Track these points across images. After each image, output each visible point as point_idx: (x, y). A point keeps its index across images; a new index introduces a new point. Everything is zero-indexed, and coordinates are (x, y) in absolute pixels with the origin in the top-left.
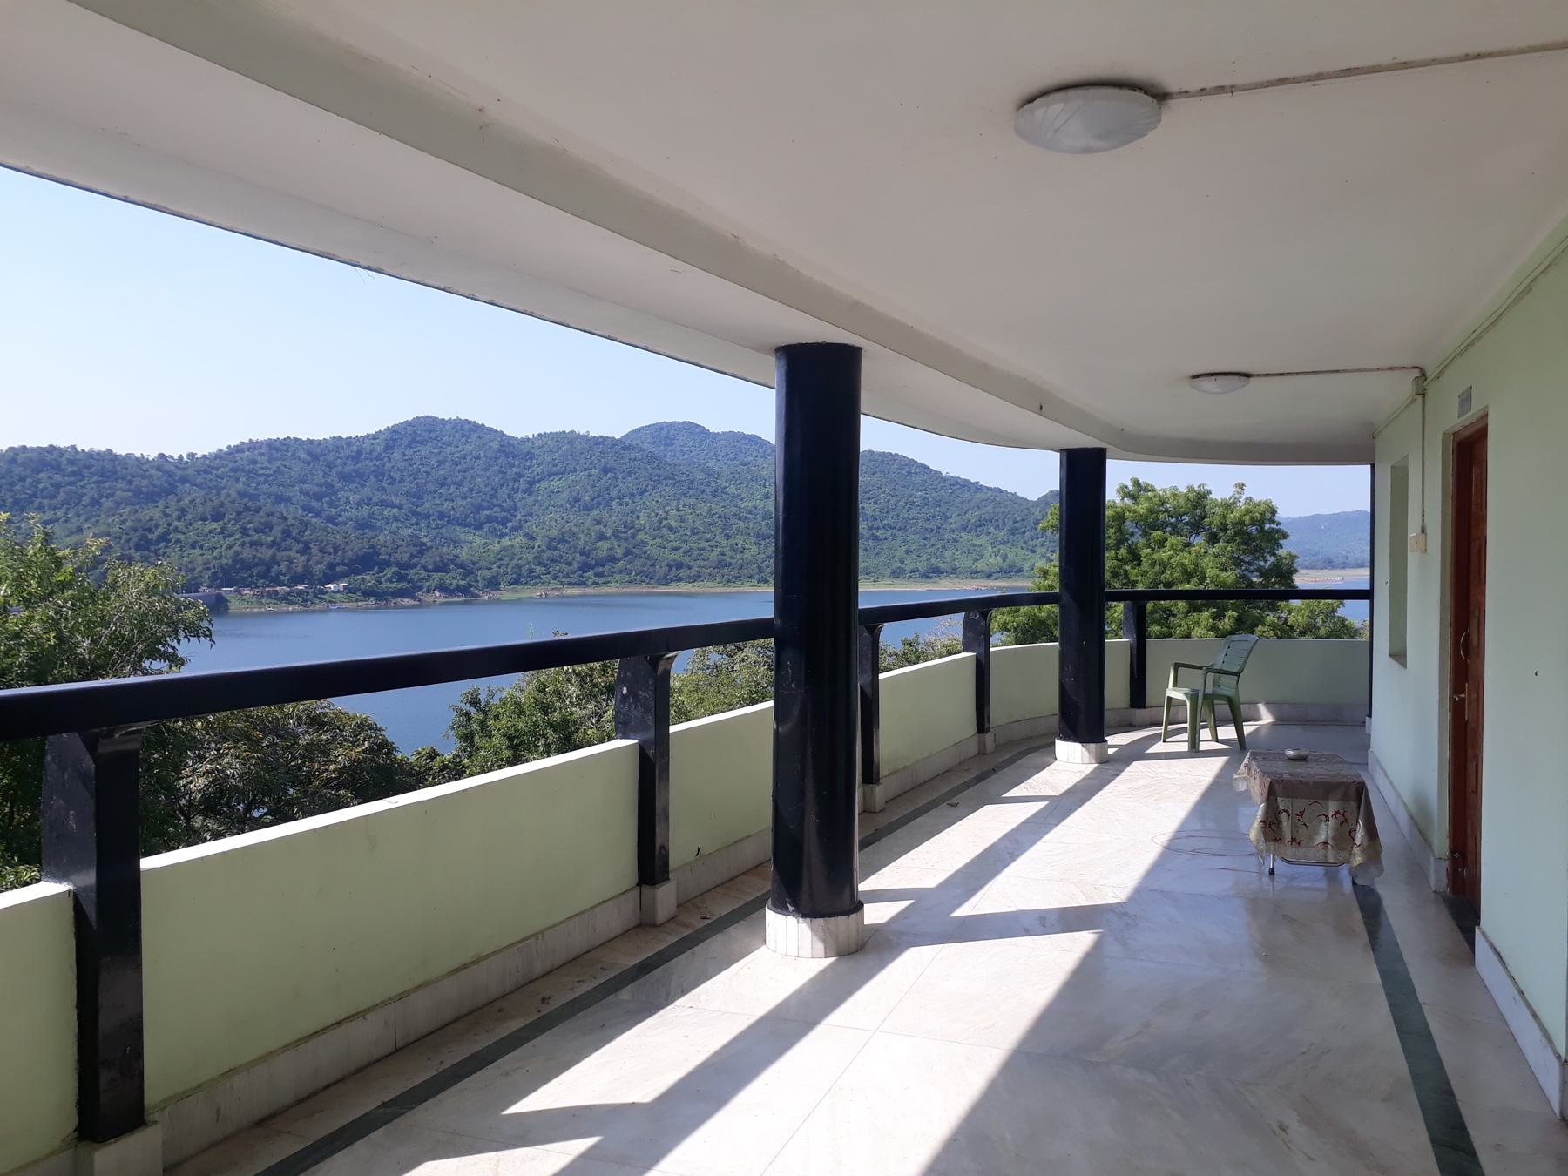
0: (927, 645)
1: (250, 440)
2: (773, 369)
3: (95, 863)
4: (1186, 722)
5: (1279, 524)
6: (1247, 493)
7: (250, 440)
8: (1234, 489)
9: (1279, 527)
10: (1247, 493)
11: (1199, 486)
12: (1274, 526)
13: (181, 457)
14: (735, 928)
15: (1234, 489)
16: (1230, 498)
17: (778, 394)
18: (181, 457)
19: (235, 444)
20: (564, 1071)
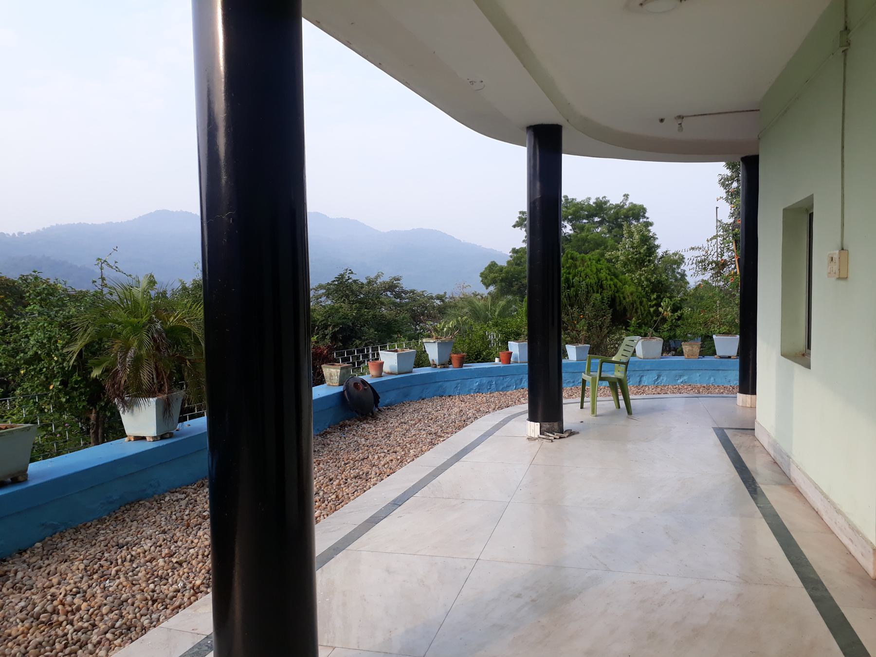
0: (451, 298)
1: (92, 224)
2: (527, 137)
3: (525, 384)
4: (586, 360)
5: (648, 218)
6: (631, 200)
7: (57, 224)
8: (623, 198)
9: (648, 220)
10: (631, 200)
11: (603, 198)
12: (645, 220)
13: (14, 234)
14: (795, 481)
15: (623, 198)
16: (621, 203)
17: (528, 149)
18: (14, 234)
19: (48, 227)
20: (136, 454)
